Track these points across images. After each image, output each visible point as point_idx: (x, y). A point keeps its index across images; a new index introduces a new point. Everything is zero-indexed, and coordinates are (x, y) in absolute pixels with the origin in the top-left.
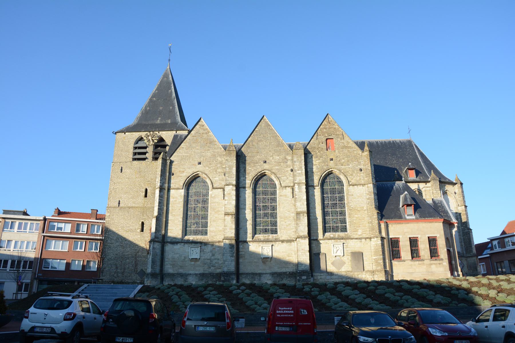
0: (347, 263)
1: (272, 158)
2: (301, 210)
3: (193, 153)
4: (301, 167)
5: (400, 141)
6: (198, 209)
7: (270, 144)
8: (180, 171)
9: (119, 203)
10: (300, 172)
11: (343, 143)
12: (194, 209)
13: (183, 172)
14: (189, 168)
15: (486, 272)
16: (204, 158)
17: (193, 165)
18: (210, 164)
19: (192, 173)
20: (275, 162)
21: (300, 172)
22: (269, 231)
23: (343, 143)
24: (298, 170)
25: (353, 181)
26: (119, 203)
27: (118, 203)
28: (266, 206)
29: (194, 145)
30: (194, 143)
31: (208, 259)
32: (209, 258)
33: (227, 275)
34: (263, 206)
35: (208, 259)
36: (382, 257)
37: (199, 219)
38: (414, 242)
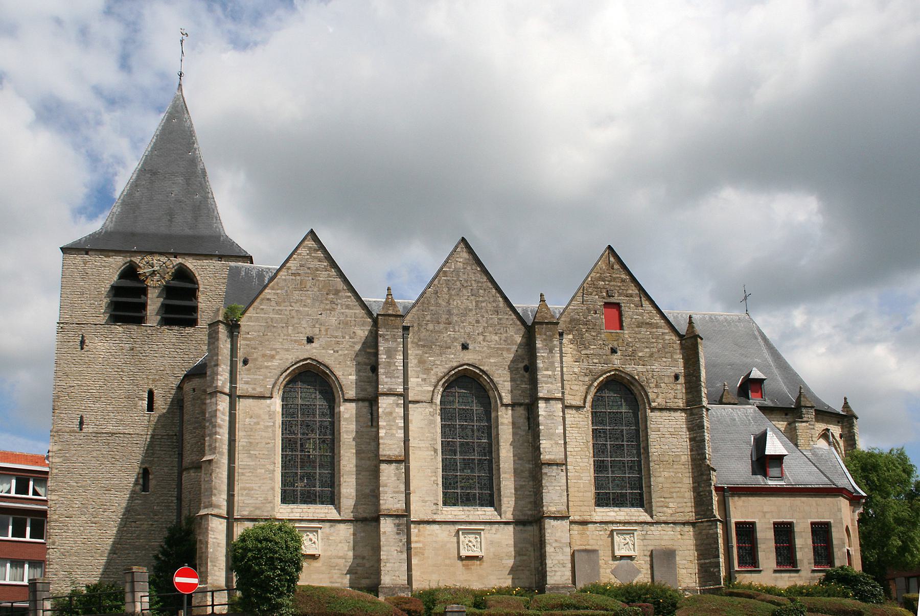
0: (644, 571)
1: (481, 338)
2: (553, 457)
3: (293, 313)
4: (553, 363)
5: (726, 320)
6: (309, 446)
7: (477, 305)
8: (264, 356)
9: (81, 423)
10: (550, 373)
11: (641, 315)
12: (302, 445)
13: (273, 357)
14: (287, 350)
15: (558, 573)
16: (323, 329)
17: (296, 341)
18: (338, 343)
19: (294, 360)
20: (489, 347)
21: (550, 373)
22: (474, 499)
23: (641, 315)
24: (547, 370)
25: (659, 400)
26: (81, 423)
27: (77, 422)
28: (467, 443)
29: (296, 295)
30: (295, 289)
31: (340, 558)
32: (341, 554)
33: (402, 589)
34: (462, 444)
35: (340, 558)
36: (413, 545)
37: (472, 470)
38: (784, 532)
